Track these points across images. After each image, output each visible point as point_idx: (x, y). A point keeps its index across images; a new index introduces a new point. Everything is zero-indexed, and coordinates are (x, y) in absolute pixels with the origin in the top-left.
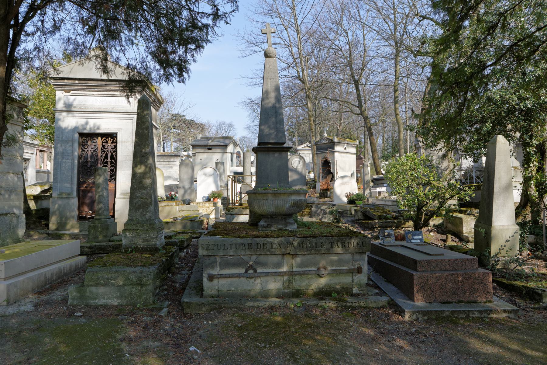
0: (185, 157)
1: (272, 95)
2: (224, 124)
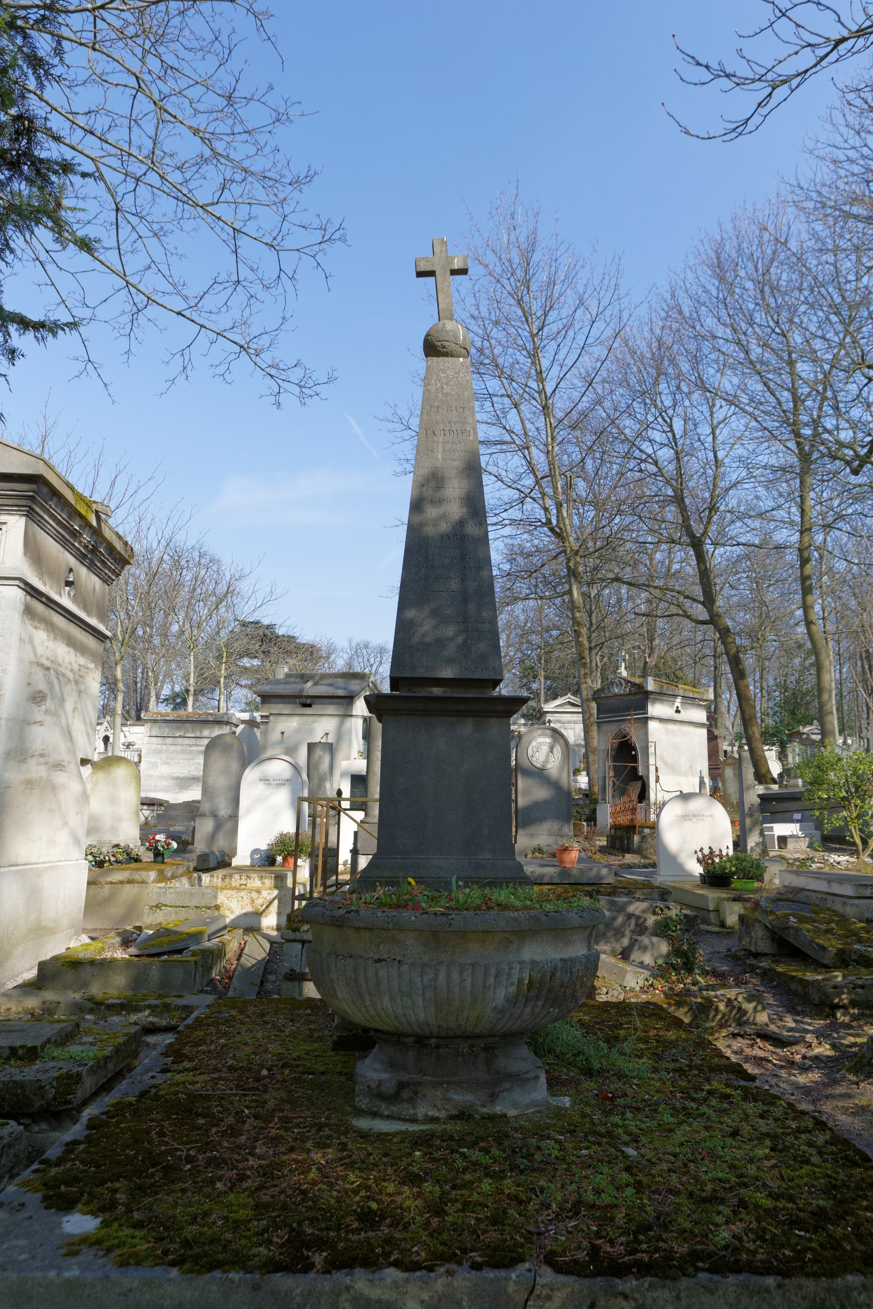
0: (242, 727)
1: (455, 489)
2: (366, 646)
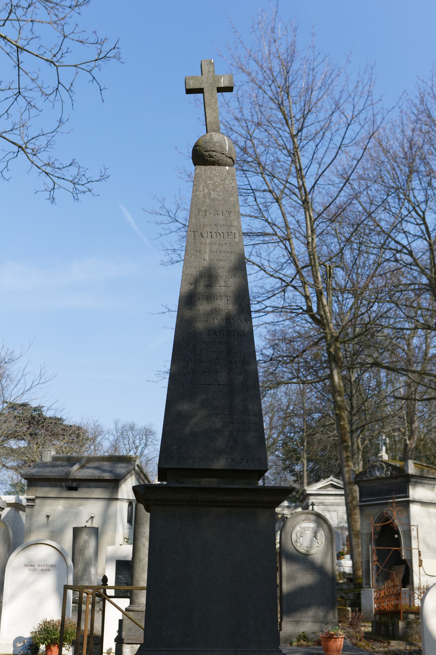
2: (132, 428)
